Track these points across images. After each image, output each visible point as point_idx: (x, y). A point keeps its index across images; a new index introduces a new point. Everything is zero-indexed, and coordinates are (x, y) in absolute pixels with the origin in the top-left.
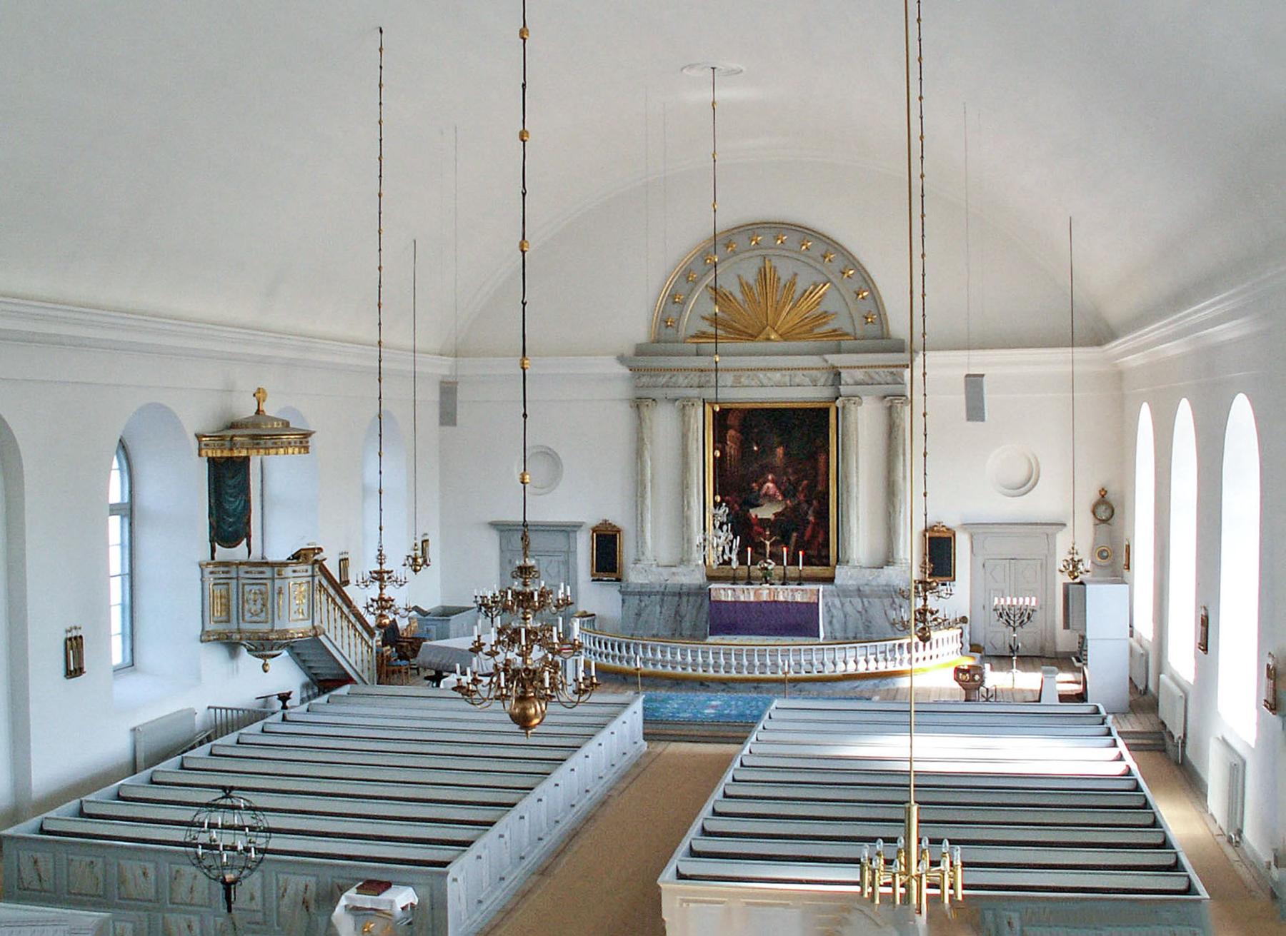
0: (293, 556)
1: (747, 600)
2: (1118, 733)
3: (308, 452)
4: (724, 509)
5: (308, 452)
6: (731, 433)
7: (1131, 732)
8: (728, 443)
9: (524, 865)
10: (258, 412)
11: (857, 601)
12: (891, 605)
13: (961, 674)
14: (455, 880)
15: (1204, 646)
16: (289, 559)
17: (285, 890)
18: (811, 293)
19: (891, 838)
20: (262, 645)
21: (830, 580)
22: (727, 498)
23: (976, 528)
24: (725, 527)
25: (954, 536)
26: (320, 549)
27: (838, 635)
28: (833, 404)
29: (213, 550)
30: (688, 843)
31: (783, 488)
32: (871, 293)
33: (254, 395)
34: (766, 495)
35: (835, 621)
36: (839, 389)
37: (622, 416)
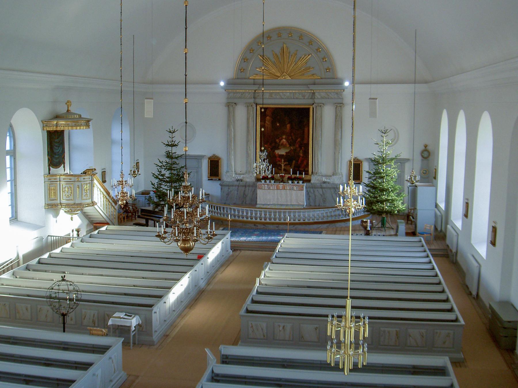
0: (83, 172)
2: (429, 249)
3: (89, 128)
4: (265, 153)
5: (89, 128)
6: (268, 118)
7: (435, 249)
9: (182, 305)
10: (68, 111)
11: (320, 190)
13: (364, 224)
14: (155, 312)
15: (466, 215)
16: (82, 173)
17: (85, 316)
19: (340, 316)
20: (71, 209)
22: (266, 146)
24: (266, 161)
25: (362, 162)
26: (95, 169)
27: (311, 204)
28: (311, 106)
29: (49, 170)
30: (251, 298)
31: (289, 142)
33: (66, 104)
34: (282, 144)
35: (311, 199)
37: (222, 112)
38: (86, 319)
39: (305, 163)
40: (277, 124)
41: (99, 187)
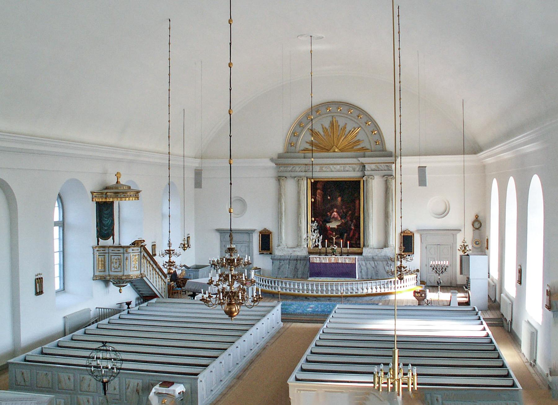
0: (132, 243)
1: (325, 262)
2: (483, 319)
3: (138, 199)
4: (316, 224)
5: (138, 199)
6: (319, 191)
8: (317, 195)
10: (117, 182)
11: (372, 263)
12: (387, 264)
13: (416, 294)
14: (201, 381)
15: (520, 282)
16: (130, 245)
17: (129, 385)
18: (353, 132)
20: (119, 281)
21: (361, 254)
23: (422, 232)
24: (316, 231)
26: (144, 241)
28: (362, 179)
30: (300, 366)
31: (340, 215)
32: (378, 132)
33: (116, 175)
34: (333, 217)
36: (364, 173)
38: (129, 388)
39: (356, 236)
40: (328, 197)
41: (149, 260)
